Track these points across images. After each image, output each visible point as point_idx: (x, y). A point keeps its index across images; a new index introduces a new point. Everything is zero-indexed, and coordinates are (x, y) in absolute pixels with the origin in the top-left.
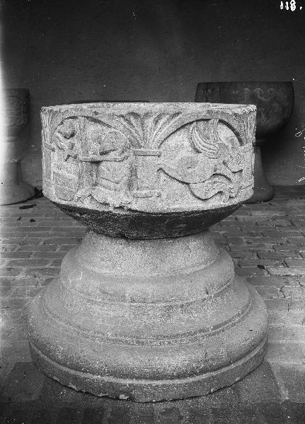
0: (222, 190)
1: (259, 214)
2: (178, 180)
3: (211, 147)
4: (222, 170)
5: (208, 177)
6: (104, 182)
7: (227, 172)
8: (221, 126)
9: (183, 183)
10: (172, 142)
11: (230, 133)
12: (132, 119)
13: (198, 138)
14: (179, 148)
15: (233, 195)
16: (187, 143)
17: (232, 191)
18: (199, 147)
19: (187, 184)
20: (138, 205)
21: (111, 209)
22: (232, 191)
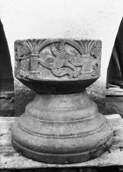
0: (68, 73)
1: (109, 87)
2: (46, 68)
3: (62, 54)
4: (68, 64)
5: (60, 67)
6: (22, 68)
7: (72, 66)
8: (66, 45)
9: (49, 69)
10: (44, 51)
11: (73, 49)
12: (29, 42)
13: (54, 49)
14: (46, 53)
15: (75, 76)
16: (50, 52)
17: (74, 74)
18: (55, 53)
19: (51, 69)
20: (31, 77)
21: (24, 78)
22: (74, 74)
